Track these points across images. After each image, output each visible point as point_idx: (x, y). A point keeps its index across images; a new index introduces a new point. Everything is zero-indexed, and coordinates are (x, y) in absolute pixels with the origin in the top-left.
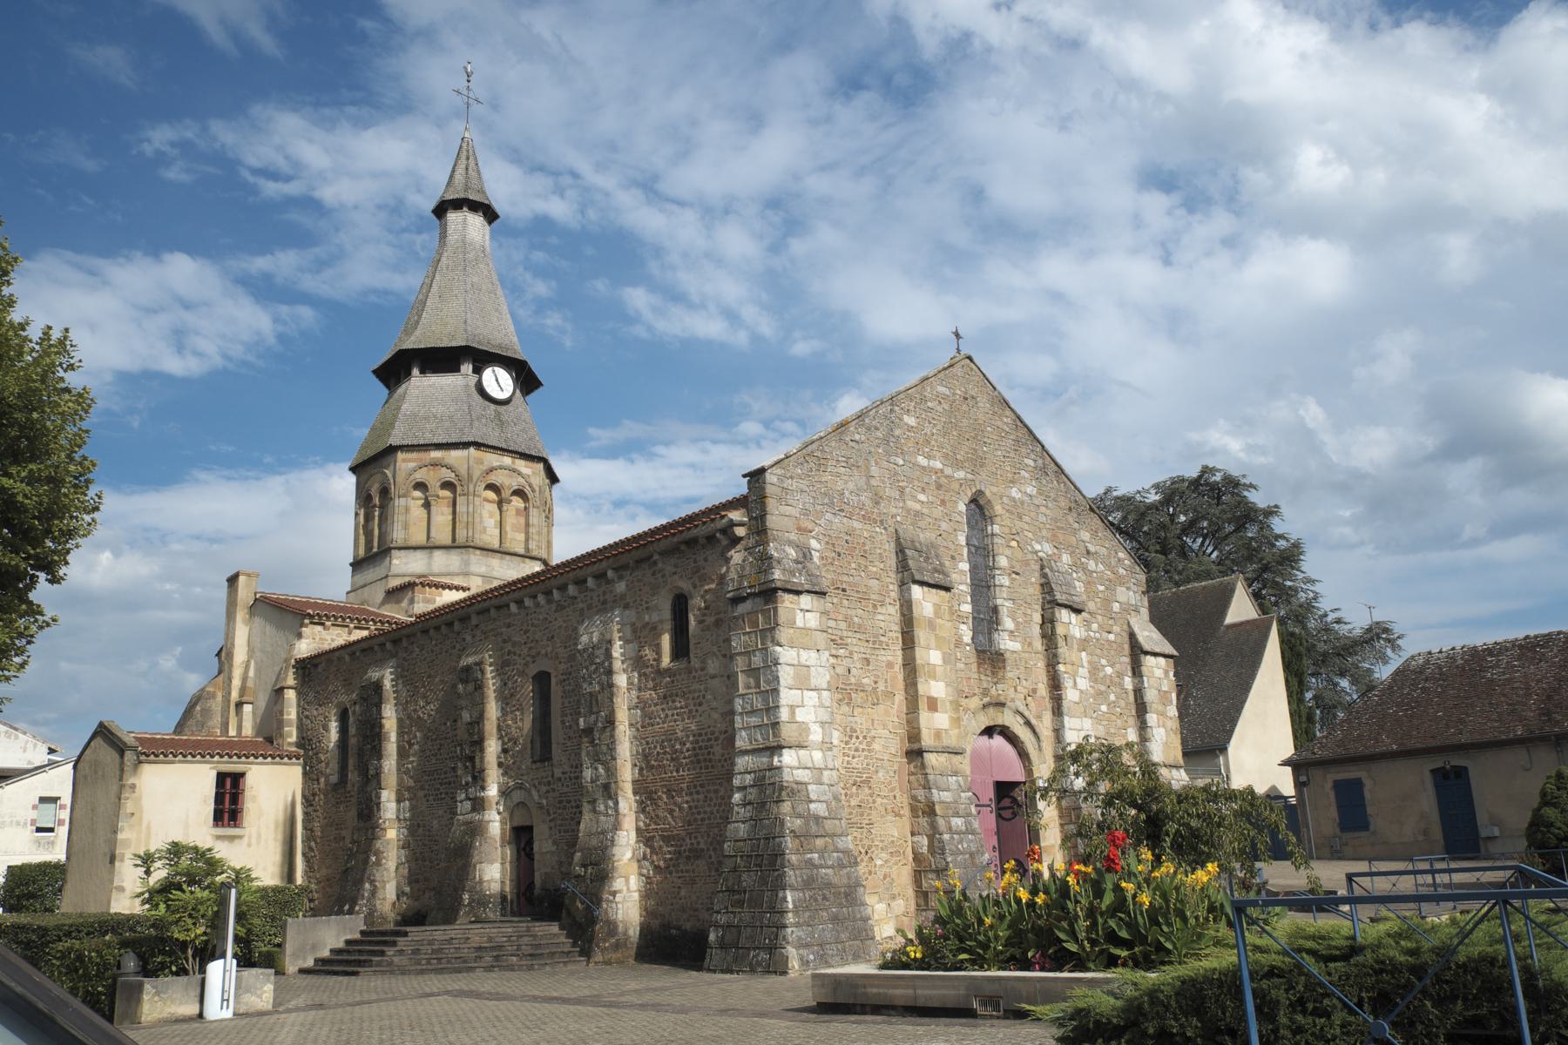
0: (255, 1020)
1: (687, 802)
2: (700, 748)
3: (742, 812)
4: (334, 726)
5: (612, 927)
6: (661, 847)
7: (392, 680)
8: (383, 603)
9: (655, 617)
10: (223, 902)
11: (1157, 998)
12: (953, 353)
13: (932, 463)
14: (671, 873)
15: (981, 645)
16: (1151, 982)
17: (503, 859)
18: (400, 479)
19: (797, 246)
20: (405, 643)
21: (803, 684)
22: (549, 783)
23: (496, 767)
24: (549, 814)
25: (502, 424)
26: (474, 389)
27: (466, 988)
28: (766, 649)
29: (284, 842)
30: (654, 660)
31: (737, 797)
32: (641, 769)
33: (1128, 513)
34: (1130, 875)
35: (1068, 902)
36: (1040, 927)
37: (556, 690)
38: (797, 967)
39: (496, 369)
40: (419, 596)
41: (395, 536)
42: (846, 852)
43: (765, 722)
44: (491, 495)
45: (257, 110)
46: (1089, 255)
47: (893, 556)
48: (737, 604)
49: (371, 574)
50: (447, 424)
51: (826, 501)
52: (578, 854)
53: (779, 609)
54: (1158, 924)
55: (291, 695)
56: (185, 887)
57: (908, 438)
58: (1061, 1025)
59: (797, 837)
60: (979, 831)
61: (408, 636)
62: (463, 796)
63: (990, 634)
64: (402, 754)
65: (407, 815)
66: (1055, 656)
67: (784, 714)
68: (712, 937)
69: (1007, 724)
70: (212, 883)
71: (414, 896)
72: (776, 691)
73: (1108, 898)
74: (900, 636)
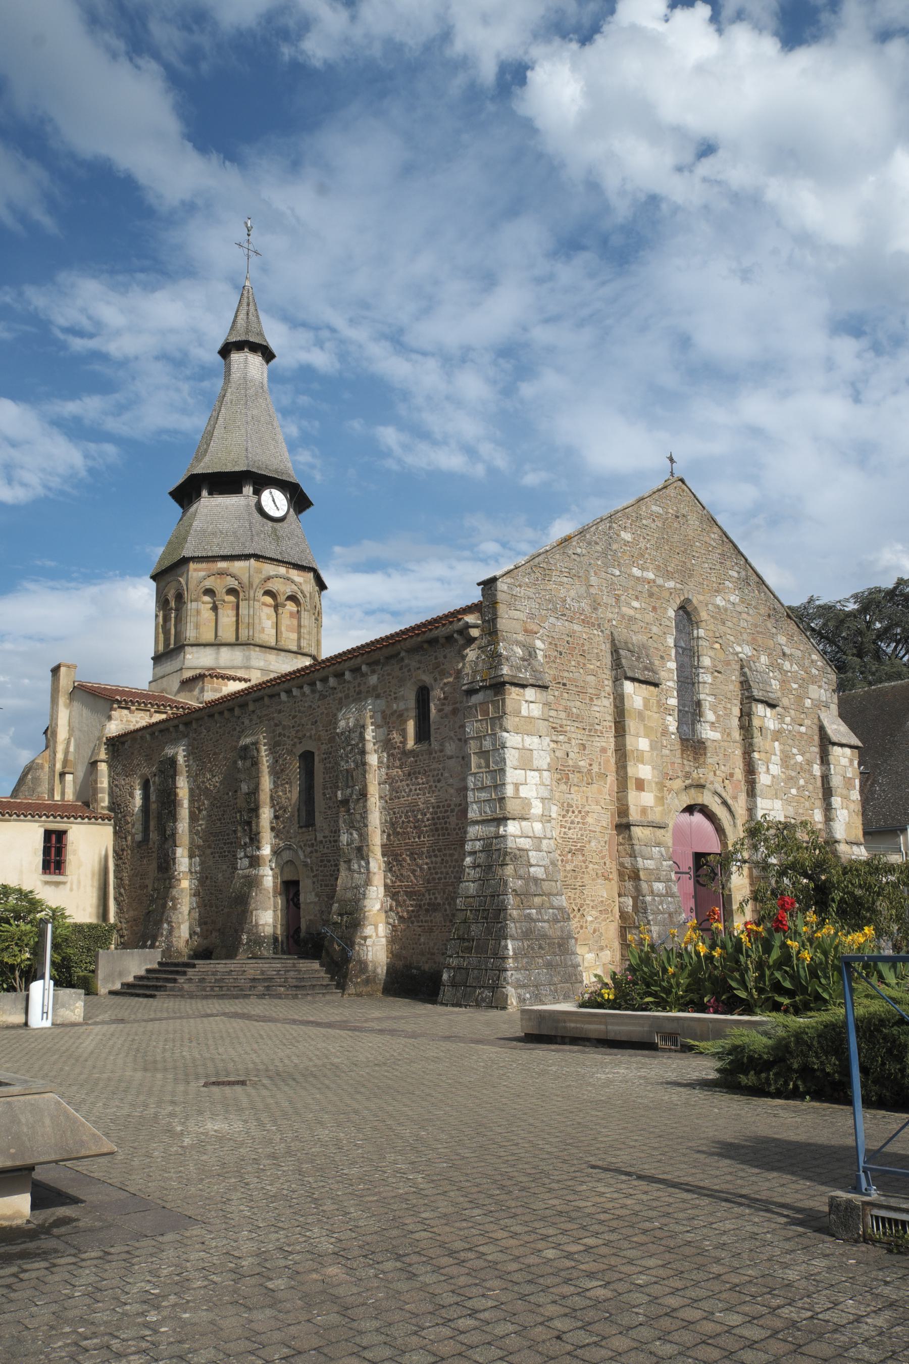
0: (69, 1029)
1: (427, 864)
2: (438, 818)
3: (472, 873)
4: (138, 794)
5: (363, 966)
6: (404, 901)
7: (185, 756)
8: (179, 691)
9: (402, 706)
10: (42, 934)
11: (802, 1038)
12: (668, 476)
13: (645, 574)
14: (412, 923)
15: (685, 735)
16: (798, 1025)
17: (275, 907)
18: (192, 585)
19: (527, 390)
20: (194, 725)
21: (526, 765)
22: (313, 845)
23: (269, 830)
24: (312, 871)
25: (278, 538)
26: (254, 508)
27: (240, 1011)
28: (495, 734)
29: (100, 889)
30: (401, 742)
31: (468, 860)
32: (389, 835)
33: (828, 620)
34: (797, 934)
35: (741, 956)
36: (716, 977)
37: (318, 767)
38: (515, 1003)
39: (273, 490)
40: (208, 686)
41: (188, 635)
42: (561, 909)
43: (493, 797)
44: (268, 600)
45: (63, 277)
46: (786, 394)
47: (609, 656)
48: (471, 696)
49: (168, 666)
50: (231, 539)
51: (550, 606)
52: (336, 905)
53: (507, 700)
54: (818, 978)
55: (103, 767)
56: (12, 921)
57: (624, 552)
58: (720, 1059)
59: (518, 895)
60: (678, 894)
61: (197, 720)
62: (242, 854)
63: (693, 724)
64: (193, 818)
65: (198, 869)
66: (751, 745)
67: (509, 791)
68: (445, 976)
69: (706, 803)
70: (34, 919)
71: (204, 935)
72: (502, 771)
73: (775, 954)
74: (613, 725)
